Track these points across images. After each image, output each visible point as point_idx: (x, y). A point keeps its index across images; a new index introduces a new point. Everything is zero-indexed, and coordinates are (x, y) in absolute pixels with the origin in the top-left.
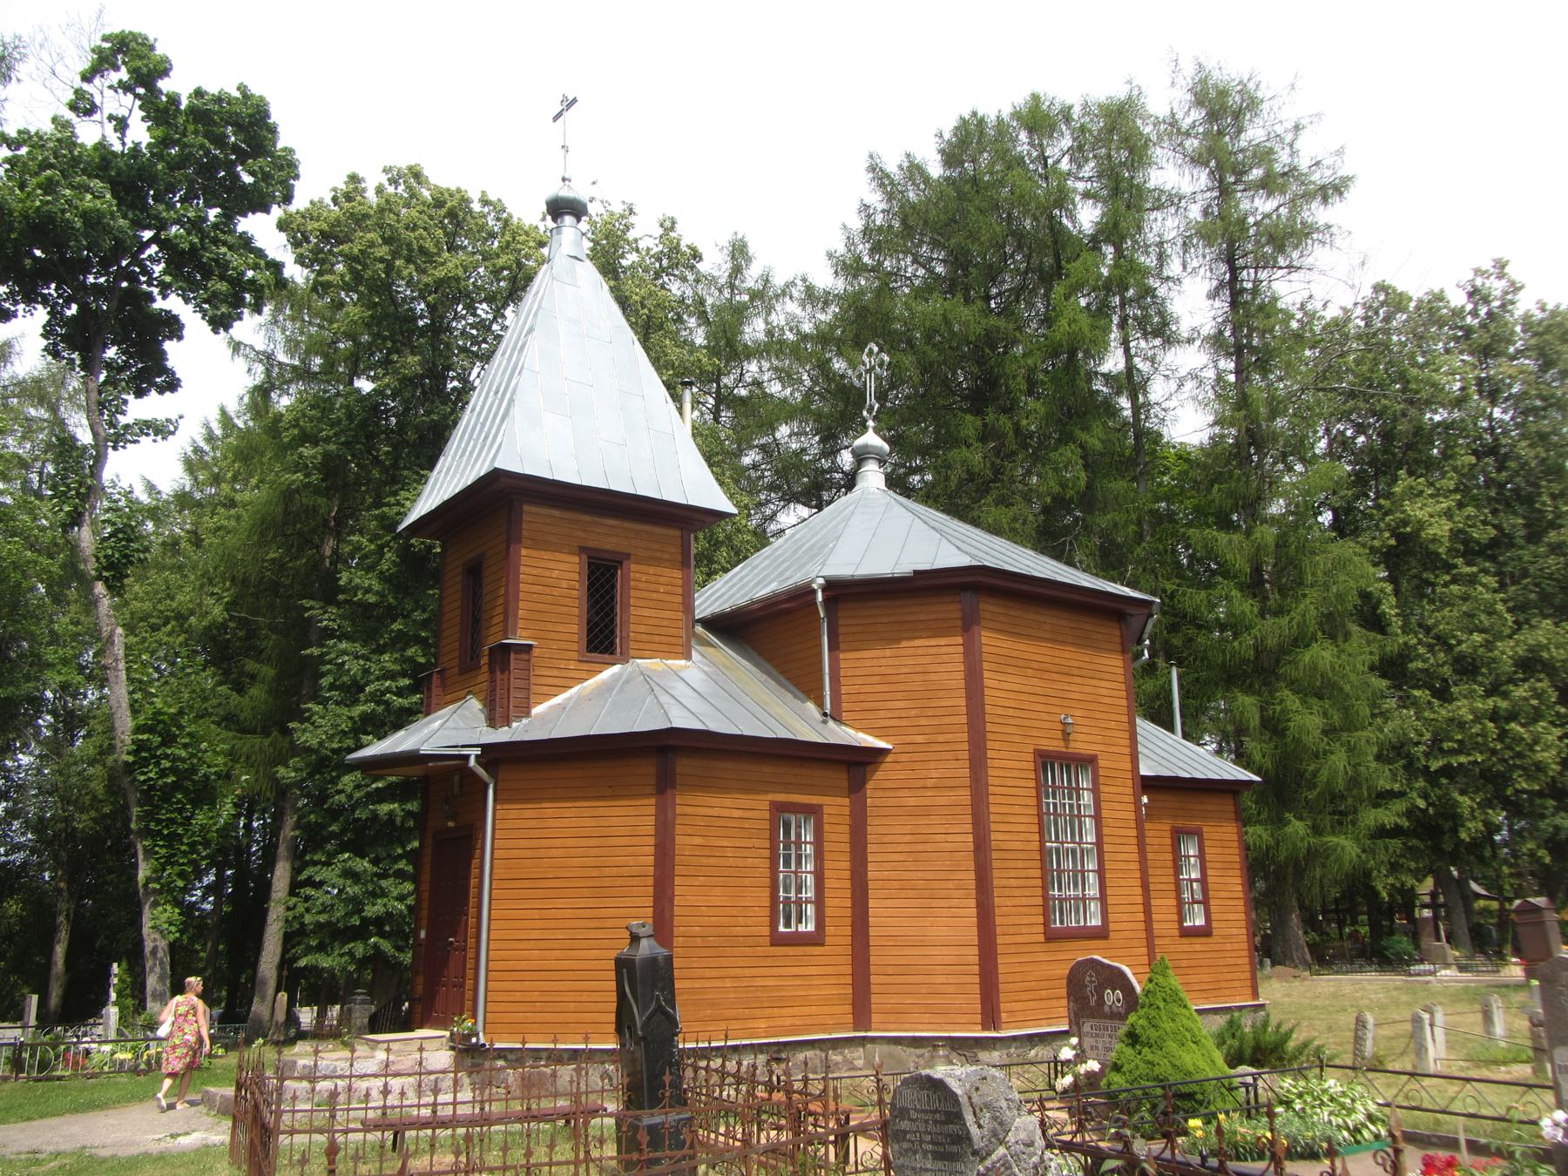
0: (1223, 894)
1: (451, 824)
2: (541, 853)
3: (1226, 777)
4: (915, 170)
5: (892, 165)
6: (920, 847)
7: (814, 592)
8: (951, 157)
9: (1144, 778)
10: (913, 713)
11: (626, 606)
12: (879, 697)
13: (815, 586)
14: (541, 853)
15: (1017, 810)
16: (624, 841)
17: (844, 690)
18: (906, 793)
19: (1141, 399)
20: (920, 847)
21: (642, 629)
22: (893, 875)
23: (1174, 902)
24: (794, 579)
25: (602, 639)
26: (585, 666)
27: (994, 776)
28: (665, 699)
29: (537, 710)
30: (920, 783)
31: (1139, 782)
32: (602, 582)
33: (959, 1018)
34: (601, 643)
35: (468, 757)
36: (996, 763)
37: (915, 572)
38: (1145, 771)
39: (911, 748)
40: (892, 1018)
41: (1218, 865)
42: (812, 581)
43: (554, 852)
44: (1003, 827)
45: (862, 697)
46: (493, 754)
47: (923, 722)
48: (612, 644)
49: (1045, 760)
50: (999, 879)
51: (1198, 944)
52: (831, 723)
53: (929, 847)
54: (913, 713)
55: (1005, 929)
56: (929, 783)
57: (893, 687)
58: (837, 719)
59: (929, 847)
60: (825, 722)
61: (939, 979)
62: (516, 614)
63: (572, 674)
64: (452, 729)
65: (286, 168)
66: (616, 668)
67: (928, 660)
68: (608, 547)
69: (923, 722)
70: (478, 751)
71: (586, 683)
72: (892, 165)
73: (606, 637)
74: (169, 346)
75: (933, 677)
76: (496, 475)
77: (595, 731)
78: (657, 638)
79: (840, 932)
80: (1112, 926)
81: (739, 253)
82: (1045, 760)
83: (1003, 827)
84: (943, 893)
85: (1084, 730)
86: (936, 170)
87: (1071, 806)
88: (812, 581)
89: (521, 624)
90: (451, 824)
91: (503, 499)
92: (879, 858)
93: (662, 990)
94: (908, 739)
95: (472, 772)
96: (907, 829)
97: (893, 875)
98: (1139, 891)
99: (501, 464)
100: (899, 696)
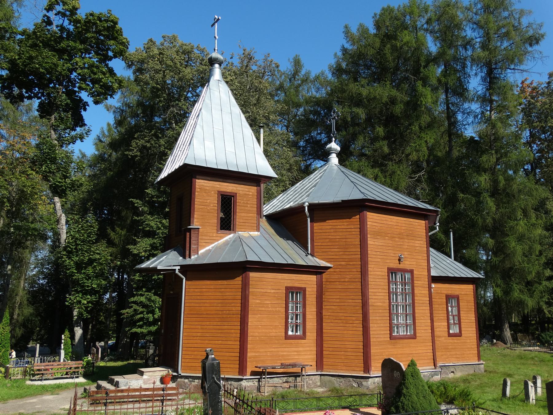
0: (466, 321)
1: (172, 292)
2: (202, 305)
3: (469, 276)
4: (363, 31)
5: (354, 30)
6: (342, 304)
7: (304, 207)
8: (378, 26)
9: (432, 276)
10: (341, 253)
11: (235, 213)
12: (328, 247)
13: (305, 205)
14: (202, 305)
15: (380, 291)
16: (230, 301)
17: (315, 244)
18: (338, 283)
19: (452, 120)
20: (342, 304)
21: (241, 221)
22: (332, 314)
23: (446, 324)
24: (299, 202)
25: (226, 224)
26: (220, 235)
27: (307, 327)
28: (246, 248)
29: (201, 252)
30: (343, 280)
31: (431, 279)
32: (227, 203)
33: (356, 369)
34: (226, 226)
35: (175, 270)
36: (372, 273)
37: (342, 201)
38: (433, 273)
39: (340, 267)
40: (331, 367)
41: (465, 309)
42: (304, 203)
43: (206, 305)
44: (374, 297)
45: (322, 247)
46: (185, 269)
47: (345, 257)
48: (230, 226)
49: (392, 272)
50: (373, 317)
51: (455, 340)
52: (310, 256)
53: (346, 304)
54: (341, 253)
55: (374, 336)
56: (347, 280)
57: (334, 244)
58: (312, 255)
59: (346, 304)
60: (307, 256)
61: (350, 354)
62: (194, 217)
63: (214, 238)
64: (169, 261)
65: (125, 45)
66: (232, 235)
67: (348, 233)
68: (228, 191)
69: (345, 257)
70: (179, 267)
71: (219, 242)
72: (354, 30)
73: (228, 224)
74: (83, 113)
75: (349, 240)
76: (185, 166)
77: (219, 261)
78: (247, 224)
79: (312, 334)
80: (417, 335)
81: (297, 63)
82: (392, 272)
83: (374, 297)
84: (351, 322)
85: (409, 260)
86: (372, 31)
87: (402, 289)
88: (304, 203)
89: (195, 220)
90: (172, 292)
91: (189, 173)
92: (328, 307)
93: (216, 375)
94: (339, 263)
95: (177, 275)
96: (338, 297)
97: (332, 314)
98: (429, 321)
99: (187, 162)
100: (336, 247)
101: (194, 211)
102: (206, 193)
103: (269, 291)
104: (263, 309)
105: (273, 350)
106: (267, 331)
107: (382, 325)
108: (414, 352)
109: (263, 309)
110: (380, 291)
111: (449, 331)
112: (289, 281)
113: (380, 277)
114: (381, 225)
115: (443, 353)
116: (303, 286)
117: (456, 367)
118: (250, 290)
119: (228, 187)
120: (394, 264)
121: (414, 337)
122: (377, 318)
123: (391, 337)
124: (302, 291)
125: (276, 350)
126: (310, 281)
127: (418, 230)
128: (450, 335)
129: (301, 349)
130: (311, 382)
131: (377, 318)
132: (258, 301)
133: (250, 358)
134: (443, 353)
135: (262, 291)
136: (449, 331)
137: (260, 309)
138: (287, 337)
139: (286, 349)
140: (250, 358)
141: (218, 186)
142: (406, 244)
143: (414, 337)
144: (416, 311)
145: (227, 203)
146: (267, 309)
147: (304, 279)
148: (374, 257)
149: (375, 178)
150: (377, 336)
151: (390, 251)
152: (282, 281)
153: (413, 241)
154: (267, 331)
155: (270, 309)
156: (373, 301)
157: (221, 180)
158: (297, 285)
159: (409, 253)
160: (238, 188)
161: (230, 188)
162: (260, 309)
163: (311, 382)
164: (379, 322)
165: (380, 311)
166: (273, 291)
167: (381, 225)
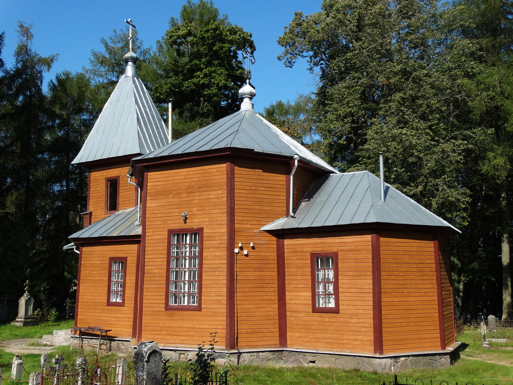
15: (158, 256)
23: (310, 294)
32: (113, 185)
44: (151, 264)
68: (113, 176)
79: (130, 304)
80: (203, 306)
101: (89, 199)
102: (98, 181)
103: (97, 262)
104: (91, 278)
105: (97, 314)
106: (93, 297)
107: (157, 294)
108: (198, 326)
109: (91, 278)
110: (158, 256)
111: (167, 303)
112: (113, 252)
113: (159, 241)
114: (165, 183)
115: (300, 335)
116: (124, 256)
117: (319, 356)
118: (82, 263)
119: (112, 173)
120: (179, 225)
121: (199, 308)
122: (152, 286)
123: (168, 308)
124: (123, 261)
125: (100, 314)
126: (130, 251)
127: (215, 177)
128: (316, 310)
129: (120, 315)
130: (123, 347)
131: (152, 286)
132: (88, 272)
133: (80, 320)
134: (300, 335)
135: (91, 262)
136: (167, 303)
137: (89, 278)
138: (109, 304)
139: (107, 315)
140: (80, 320)
141: (106, 174)
142: (197, 198)
143: (199, 308)
144: (204, 278)
145: (113, 185)
146: (94, 278)
147: (124, 249)
148: (154, 219)
149: (201, 126)
150: (150, 306)
151: (174, 211)
152: (107, 253)
153: (208, 193)
154: (93, 297)
155: (97, 278)
156: (149, 267)
157: (100, 169)
158: (119, 255)
159: (200, 208)
160: (121, 171)
161: (115, 172)
162: (89, 278)
163: (123, 347)
164: (154, 290)
165: (157, 278)
166: (99, 262)
167: (165, 183)
